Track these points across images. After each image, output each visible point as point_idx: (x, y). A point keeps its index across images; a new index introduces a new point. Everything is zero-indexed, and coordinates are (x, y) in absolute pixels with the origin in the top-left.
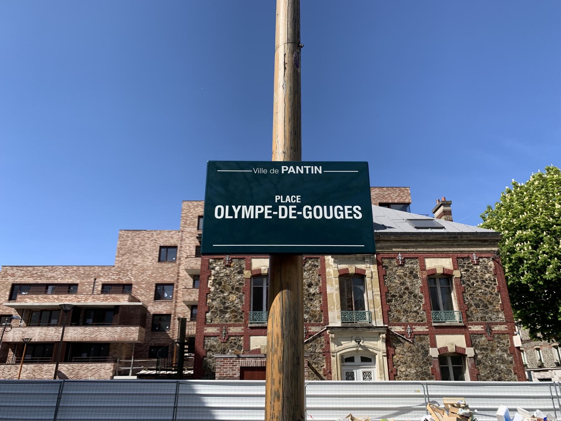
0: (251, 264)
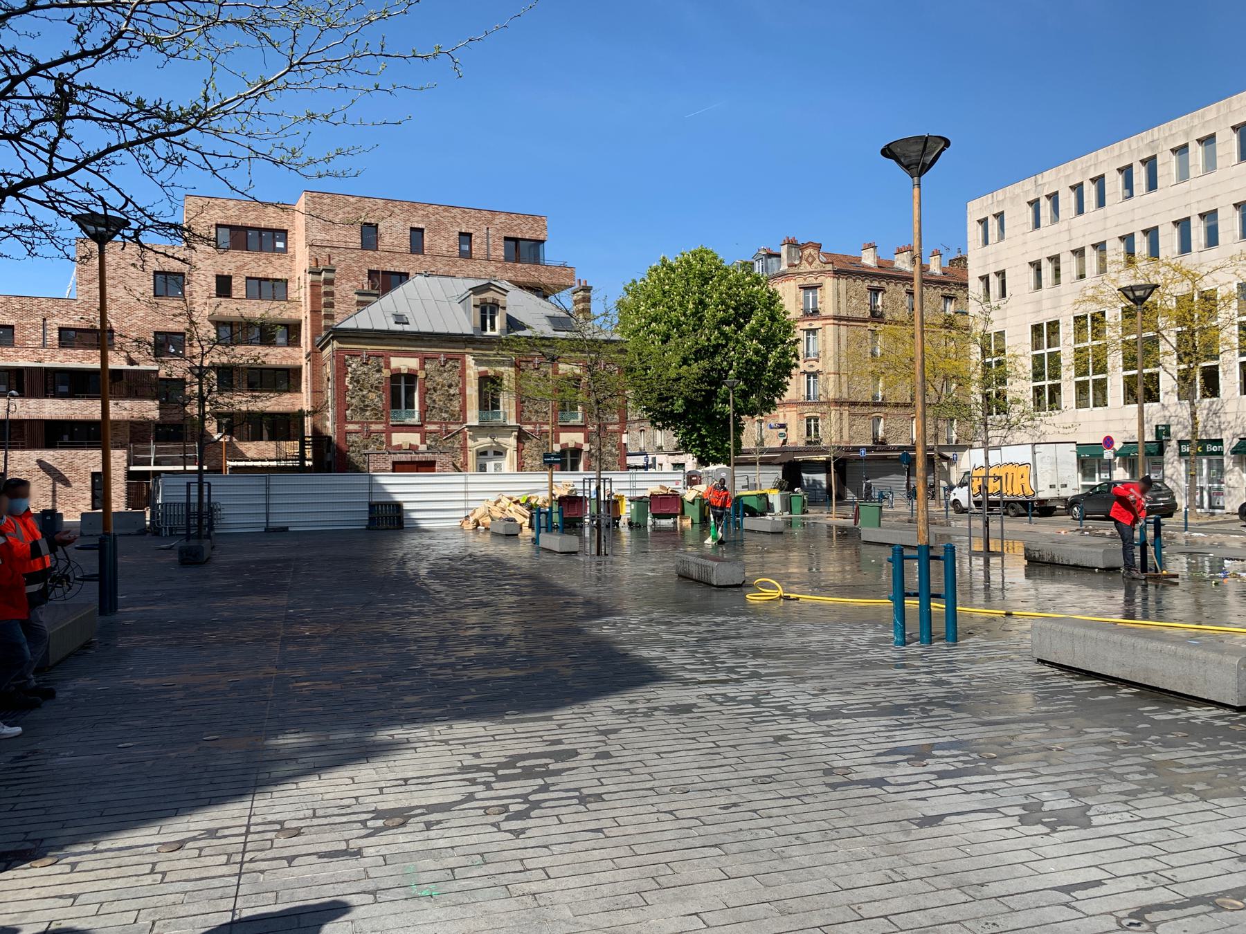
0: (389, 363)
